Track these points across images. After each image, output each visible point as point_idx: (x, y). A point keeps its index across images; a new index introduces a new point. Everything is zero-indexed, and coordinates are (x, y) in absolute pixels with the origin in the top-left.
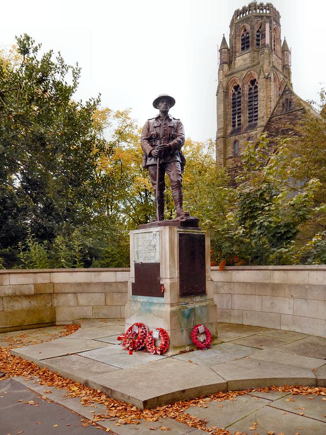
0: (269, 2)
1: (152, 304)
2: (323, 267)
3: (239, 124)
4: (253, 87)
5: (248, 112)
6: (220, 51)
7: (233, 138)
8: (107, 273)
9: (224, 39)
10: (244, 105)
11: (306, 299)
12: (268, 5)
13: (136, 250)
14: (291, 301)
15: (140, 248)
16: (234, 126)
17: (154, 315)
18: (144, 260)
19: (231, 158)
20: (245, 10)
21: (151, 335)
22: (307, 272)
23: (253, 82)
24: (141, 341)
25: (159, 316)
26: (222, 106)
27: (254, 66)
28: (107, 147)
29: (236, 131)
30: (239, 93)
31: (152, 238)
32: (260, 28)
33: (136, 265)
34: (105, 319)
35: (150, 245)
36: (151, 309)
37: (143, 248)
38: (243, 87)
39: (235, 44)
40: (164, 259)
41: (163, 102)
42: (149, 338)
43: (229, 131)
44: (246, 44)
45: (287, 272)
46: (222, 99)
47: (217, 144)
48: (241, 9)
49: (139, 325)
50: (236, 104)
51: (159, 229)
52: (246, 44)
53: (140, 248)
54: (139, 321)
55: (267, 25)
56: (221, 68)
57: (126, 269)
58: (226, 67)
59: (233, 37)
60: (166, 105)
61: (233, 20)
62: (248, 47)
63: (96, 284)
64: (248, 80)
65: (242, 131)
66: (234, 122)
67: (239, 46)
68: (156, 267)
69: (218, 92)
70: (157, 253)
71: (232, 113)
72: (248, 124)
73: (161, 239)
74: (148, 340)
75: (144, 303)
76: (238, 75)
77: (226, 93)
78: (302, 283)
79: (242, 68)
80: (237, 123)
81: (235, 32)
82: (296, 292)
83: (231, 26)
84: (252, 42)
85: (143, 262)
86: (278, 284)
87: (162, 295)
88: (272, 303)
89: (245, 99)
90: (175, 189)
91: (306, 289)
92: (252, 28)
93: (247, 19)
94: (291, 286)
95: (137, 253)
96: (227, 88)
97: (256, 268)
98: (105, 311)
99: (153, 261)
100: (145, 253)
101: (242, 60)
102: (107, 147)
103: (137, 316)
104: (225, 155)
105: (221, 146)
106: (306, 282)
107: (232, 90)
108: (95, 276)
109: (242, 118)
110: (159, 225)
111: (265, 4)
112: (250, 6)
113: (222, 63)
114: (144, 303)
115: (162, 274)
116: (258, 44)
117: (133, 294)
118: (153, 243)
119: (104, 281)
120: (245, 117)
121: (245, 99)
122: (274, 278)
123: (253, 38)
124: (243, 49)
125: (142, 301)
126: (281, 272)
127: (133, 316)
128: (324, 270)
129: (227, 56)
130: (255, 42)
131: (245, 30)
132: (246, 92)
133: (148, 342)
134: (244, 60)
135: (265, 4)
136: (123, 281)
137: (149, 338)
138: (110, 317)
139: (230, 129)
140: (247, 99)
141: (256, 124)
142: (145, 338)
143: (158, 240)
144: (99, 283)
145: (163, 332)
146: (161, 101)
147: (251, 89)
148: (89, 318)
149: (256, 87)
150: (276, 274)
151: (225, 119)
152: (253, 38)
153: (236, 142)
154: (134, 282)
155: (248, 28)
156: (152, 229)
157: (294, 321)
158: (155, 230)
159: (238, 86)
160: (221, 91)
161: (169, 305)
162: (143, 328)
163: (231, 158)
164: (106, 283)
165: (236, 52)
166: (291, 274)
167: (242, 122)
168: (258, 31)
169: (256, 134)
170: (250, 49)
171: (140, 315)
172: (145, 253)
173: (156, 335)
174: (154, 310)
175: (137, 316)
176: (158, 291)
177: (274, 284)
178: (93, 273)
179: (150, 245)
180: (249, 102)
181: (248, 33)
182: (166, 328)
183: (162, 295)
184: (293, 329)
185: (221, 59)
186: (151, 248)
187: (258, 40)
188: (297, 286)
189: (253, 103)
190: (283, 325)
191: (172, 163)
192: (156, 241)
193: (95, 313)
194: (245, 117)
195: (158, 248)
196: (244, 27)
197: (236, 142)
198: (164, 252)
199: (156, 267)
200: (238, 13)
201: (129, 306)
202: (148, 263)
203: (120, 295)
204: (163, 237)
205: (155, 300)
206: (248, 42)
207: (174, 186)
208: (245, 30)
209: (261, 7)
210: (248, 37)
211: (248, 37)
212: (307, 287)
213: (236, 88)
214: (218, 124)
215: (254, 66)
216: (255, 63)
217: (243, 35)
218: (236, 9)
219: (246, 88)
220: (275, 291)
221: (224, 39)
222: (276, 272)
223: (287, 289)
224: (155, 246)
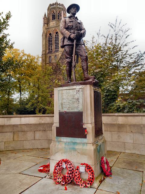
0: (62, 3)
1: (75, 143)
2: (144, 114)
3: (51, 50)
4: (57, 35)
5: (55, 45)
6: (44, 18)
7: (49, 55)
8: (15, 118)
9: (45, 14)
10: (53, 42)
11: (142, 133)
12: (62, 4)
13: (60, 102)
14: (132, 134)
15: (64, 101)
16: (49, 50)
17: (78, 152)
18: (68, 109)
19: (48, 63)
20: (53, 5)
21: (77, 169)
22: (141, 117)
23: (57, 33)
24: (71, 175)
25: (83, 153)
26: (44, 41)
27: (57, 26)
28: (10, 44)
29: (50, 52)
30: (51, 36)
31: (75, 93)
32: (59, 12)
33: (62, 116)
34: (13, 151)
35: (73, 99)
36: (75, 147)
37: (67, 101)
38: (53, 34)
39: (50, 17)
40: (85, 109)
41: (74, 8)
42: (76, 172)
43: (47, 52)
44: (54, 17)
45: (127, 117)
46: (44, 38)
47: (42, 57)
48: (52, 4)
49: (66, 162)
50: (50, 41)
51: (81, 86)
52: (54, 17)
53: (64, 101)
54: (65, 158)
55: (62, 12)
56: (44, 26)
57: (51, 115)
58: (46, 25)
59: (49, 14)
60: (76, 10)
61: (49, 7)
62: (55, 19)
63: (8, 126)
64: (55, 32)
65: (53, 52)
66: (49, 48)
67: (51, 18)
68: (80, 115)
69: (43, 35)
70: (80, 105)
71: (48, 44)
72: (55, 50)
73: (83, 94)
74: (76, 174)
75: (67, 143)
76: (51, 29)
77: (46, 36)
78: (137, 124)
79: (53, 26)
80: (50, 49)
81: (50, 12)
82: (135, 129)
83: (48, 10)
84: (57, 17)
85: (67, 111)
86: (122, 125)
87: (85, 137)
88: (119, 136)
89: (54, 39)
90: (85, 62)
91: (141, 128)
92: (56, 12)
93: (54, 8)
94: (130, 125)
95: (62, 104)
96: (47, 34)
97: (107, 115)
98: (13, 145)
99: (76, 110)
100: (69, 104)
101: (52, 24)
102: (10, 44)
103: (62, 153)
104: (45, 62)
105: (44, 58)
106: (141, 123)
107: (48, 35)
108: (7, 120)
109: (52, 47)
110: (81, 84)
111: (61, 4)
112: (55, 3)
113: (44, 24)
114: (67, 143)
115: (84, 121)
116: (59, 19)
117: (57, 136)
118: (76, 97)
119: (13, 124)
120: (54, 47)
121: (54, 39)
122: (119, 121)
123: (57, 16)
124: (53, 19)
125: (65, 141)
126: (124, 117)
127: (57, 153)
128: (144, 116)
129: (47, 21)
130: (58, 17)
131: (54, 12)
132: (54, 37)
133: (76, 176)
134: (54, 24)
135: (61, 4)
136: (25, 123)
137: (76, 172)
138: (16, 149)
139: (48, 51)
140: (54, 39)
141: (58, 50)
142: (73, 172)
143: (81, 95)
144: (10, 126)
145: (88, 167)
146: (73, 7)
147: (56, 36)
148: (2, 150)
149: (58, 35)
150: (120, 118)
151: (46, 47)
152: (57, 16)
153: (50, 57)
154: (58, 126)
155: (55, 12)
156: (74, 87)
157: (134, 147)
158: (78, 87)
159: (51, 34)
160: (44, 35)
161: (92, 144)
162: (69, 163)
163: (48, 63)
164: (14, 126)
165: (50, 20)
166: (130, 118)
167: (52, 48)
168: (58, 14)
169: (58, 54)
170: (56, 20)
171: (65, 152)
172: (69, 104)
173: (82, 169)
174: (78, 149)
175: (62, 153)
176: (82, 134)
177: (119, 124)
178: (6, 119)
179: (73, 99)
180: (55, 41)
181: (55, 13)
182: (90, 163)
183: (85, 137)
184: (133, 152)
185: (44, 21)
186: (74, 100)
187: (59, 17)
188: (134, 125)
189: (57, 41)
190: (126, 149)
191: (80, 45)
192: (80, 95)
193: (6, 147)
194: (54, 47)
195: (81, 100)
196: (53, 11)
197: (50, 57)
198: (85, 104)
199: (80, 115)
200: (51, 5)
201: (54, 146)
202: (71, 112)
203: (23, 133)
204: (85, 93)
205: (78, 140)
206: (55, 17)
207: (84, 59)
208: (54, 12)
209: (59, 4)
210: (55, 15)
211: (55, 15)
212: (142, 126)
213: (50, 34)
214: (43, 48)
215: (57, 26)
216: (58, 25)
217: (53, 14)
218: (50, 3)
219: (54, 35)
220: (120, 129)
221: (45, 14)
222: (120, 117)
223: (128, 127)
224: (78, 99)
